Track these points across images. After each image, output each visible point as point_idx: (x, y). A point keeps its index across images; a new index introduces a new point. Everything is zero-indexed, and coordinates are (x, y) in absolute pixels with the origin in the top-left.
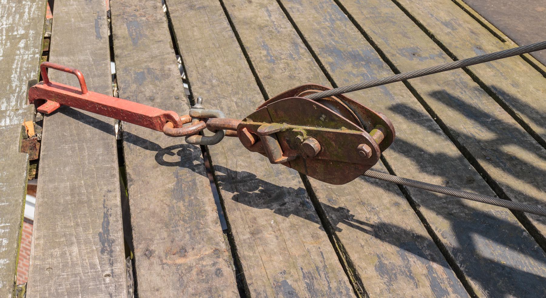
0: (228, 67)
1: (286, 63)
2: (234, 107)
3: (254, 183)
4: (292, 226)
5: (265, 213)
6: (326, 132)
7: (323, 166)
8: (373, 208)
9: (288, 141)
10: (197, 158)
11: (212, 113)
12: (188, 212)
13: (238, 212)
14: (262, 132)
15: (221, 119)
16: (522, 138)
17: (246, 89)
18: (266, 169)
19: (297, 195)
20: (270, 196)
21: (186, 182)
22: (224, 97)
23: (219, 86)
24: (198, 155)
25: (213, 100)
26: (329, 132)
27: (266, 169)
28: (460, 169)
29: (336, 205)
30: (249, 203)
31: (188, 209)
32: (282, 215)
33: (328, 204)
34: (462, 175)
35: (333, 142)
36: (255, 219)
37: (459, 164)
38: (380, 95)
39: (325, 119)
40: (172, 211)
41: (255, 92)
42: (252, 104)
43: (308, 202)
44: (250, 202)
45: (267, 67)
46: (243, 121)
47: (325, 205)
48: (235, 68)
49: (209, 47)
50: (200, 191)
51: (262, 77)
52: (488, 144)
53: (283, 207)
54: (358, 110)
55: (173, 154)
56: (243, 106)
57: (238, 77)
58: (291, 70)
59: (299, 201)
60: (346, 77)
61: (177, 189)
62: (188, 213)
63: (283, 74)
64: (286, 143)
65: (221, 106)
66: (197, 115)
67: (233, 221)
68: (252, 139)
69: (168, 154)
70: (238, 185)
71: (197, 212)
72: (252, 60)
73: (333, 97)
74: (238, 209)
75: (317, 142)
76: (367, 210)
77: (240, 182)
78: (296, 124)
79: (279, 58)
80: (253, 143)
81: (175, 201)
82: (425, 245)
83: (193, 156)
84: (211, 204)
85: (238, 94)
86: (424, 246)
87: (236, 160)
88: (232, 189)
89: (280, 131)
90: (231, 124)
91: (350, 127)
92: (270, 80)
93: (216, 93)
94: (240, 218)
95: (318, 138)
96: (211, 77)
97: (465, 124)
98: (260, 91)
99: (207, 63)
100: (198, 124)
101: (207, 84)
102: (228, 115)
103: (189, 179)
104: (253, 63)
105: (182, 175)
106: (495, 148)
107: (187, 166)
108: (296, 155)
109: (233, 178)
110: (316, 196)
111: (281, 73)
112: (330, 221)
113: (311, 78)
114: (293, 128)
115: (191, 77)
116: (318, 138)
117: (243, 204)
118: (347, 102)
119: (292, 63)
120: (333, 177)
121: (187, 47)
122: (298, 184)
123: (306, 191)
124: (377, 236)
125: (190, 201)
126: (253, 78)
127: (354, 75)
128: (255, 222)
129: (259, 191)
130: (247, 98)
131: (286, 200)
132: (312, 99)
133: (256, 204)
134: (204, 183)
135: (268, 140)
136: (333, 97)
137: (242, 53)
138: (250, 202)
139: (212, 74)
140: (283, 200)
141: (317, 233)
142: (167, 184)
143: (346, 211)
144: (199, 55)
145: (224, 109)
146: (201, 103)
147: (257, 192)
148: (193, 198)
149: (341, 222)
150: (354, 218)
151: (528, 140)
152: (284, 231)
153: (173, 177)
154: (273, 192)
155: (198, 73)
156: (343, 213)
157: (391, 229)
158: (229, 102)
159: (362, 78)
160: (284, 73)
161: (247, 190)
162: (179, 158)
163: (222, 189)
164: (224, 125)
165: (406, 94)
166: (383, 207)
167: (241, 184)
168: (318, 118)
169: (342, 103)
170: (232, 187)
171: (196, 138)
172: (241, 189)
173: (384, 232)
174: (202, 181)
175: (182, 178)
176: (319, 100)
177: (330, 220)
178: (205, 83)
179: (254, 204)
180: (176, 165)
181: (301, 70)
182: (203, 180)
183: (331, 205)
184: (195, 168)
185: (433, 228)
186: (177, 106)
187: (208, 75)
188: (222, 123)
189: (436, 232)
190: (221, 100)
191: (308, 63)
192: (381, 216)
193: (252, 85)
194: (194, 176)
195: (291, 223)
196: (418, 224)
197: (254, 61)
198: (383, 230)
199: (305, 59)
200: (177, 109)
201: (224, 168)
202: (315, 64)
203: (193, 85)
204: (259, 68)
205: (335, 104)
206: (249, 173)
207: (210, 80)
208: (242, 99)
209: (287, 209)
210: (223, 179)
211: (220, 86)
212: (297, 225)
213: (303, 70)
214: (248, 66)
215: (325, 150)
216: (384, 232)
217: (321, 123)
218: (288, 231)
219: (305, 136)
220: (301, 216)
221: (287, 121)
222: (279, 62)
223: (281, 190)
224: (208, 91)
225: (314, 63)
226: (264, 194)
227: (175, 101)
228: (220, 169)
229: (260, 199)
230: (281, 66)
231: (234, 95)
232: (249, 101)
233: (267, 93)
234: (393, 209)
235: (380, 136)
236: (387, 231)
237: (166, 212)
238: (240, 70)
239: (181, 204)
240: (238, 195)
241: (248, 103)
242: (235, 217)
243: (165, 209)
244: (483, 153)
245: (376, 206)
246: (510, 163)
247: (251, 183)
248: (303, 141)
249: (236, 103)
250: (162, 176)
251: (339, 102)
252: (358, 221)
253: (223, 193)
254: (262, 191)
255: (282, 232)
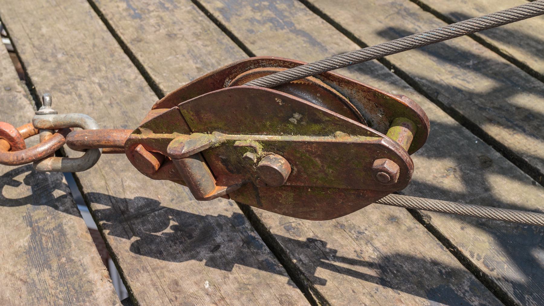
0: (75, 33)
1: (158, 16)
2: (98, 92)
3: (159, 216)
4: (242, 287)
5: (191, 270)
6: (304, 143)
7: (292, 194)
8: (360, 233)
9: (224, 161)
10: (58, 186)
11: (72, 121)
12: (61, 288)
13: (145, 275)
14: (177, 153)
15: (93, 131)
16: (527, 85)
17: (110, 63)
18: (171, 188)
19: (233, 226)
20: (190, 237)
21: (47, 231)
22: (80, 79)
23: (68, 62)
24: (57, 180)
25: (64, 85)
26: (309, 143)
27: (171, 188)
28: (463, 145)
29: (300, 236)
30: (159, 255)
31: (60, 284)
32: (220, 269)
33: (287, 235)
34: (470, 154)
35: (317, 159)
36: (176, 283)
37: (458, 136)
38: (305, 47)
39: (299, 121)
40: (33, 291)
41: (124, 65)
42: (124, 84)
43: (254, 238)
44: (161, 253)
45: (132, 26)
46: (134, 133)
47: (283, 238)
48: (86, 33)
49: (43, 7)
50: (73, 245)
51: (129, 41)
52: (485, 100)
53: (217, 254)
54: (357, 95)
55: (17, 184)
56: (111, 89)
57: (94, 45)
58: (167, 26)
59: (240, 238)
60: (249, 26)
61: (35, 248)
62: (61, 291)
63: (157, 33)
64: (220, 165)
65: (78, 93)
66: (47, 125)
67: (141, 293)
68: (155, 162)
69: (9, 184)
70: (134, 224)
71: (76, 286)
72: (108, 17)
73: (311, 78)
74: (144, 269)
75: (284, 161)
76: (351, 237)
77: (136, 217)
78: (238, 132)
79: (146, 11)
80: (157, 168)
81: (34, 271)
82: (467, 288)
83: (50, 183)
84: (98, 268)
85: (100, 70)
86: (466, 291)
87: (120, 179)
88: (126, 232)
89: (211, 148)
90: (111, 139)
91: (353, 131)
92: (141, 44)
93: (66, 72)
94: (151, 286)
95: (286, 154)
96: (54, 51)
97: (439, 74)
98: (130, 63)
99: (44, 30)
100: (51, 140)
101: (50, 62)
102: (92, 106)
103: (52, 226)
104: (111, 22)
105: (39, 219)
106: (496, 105)
107: (44, 201)
108: (240, 182)
109: (123, 212)
110: (263, 225)
111: (155, 32)
112: (301, 268)
113: (199, 34)
114: (235, 141)
115: (24, 53)
116: (286, 154)
117: (149, 258)
118: (335, 83)
119: (166, 15)
120: (313, 209)
121: (10, 10)
122: (229, 207)
123: (246, 219)
124: (383, 282)
125: (61, 267)
126: (116, 45)
127: (258, 22)
128: (178, 289)
129: (171, 228)
130: (114, 75)
131: (219, 239)
132: (268, 87)
133: (172, 254)
134: (78, 229)
135: (188, 164)
136: (311, 78)
137: (92, 11)
138: (161, 253)
139: (55, 45)
140: (214, 240)
141: (286, 295)
142: (16, 240)
143: (319, 245)
144: (31, 20)
145: (83, 97)
146: (50, 104)
147: (168, 230)
148: (64, 260)
149: (318, 266)
150: (338, 254)
151: (536, 86)
152: (230, 300)
153: (24, 225)
154: (193, 227)
155: (34, 46)
156: (315, 249)
157: (402, 267)
158: (88, 86)
159: (271, 24)
160: (159, 30)
161: (150, 230)
162: (28, 190)
163: (109, 234)
164: (98, 141)
165: (341, 40)
166: (374, 228)
167: (139, 220)
168: (285, 120)
169: (325, 86)
170: (124, 228)
171: (53, 163)
172: (140, 230)
173: (393, 273)
174: (73, 226)
175: (40, 225)
176: (280, 86)
177: (299, 265)
178: (46, 61)
179: (167, 255)
180: (26, 204)
181: (182, 23)
182: (76, 224)
183: (292, 238)
184: (57, 203)
185: (467, 254)
186: (10, 101)
187: (49, 48)
188: (96, 138)
189: (474, 261)
190: (76, 82)
191: (189, 12)
192: (378, 244)
193: (116, 54)
194: (59, 218)
195: (238, 282)
196: (439, 250)
197: (111, 19)
198: (390, 269)
199: (183, 7)
200: (11, 106)
201: (105, 195)
202: (199, 13)
203: (29, 65)
204: (120, 28)
205: (313, 89)
206: (147, 199)
207: (54, 56)
208: (107, 78)
209: (224, 256)
210: (106, 216)
211: (71, 62)
212: (250, 285)
213: (185, 23)
214: (105, 28)
215: (299, 171)
216: (393, 273)
217: (291, 127)
218: (239, 299)
219: (260, 152)
220: (251, 266)
221: (221, 128)
222: (147, 16)
223: (205, 221)
224: (54, 72)
225: (197, 11)
226: (179, 233)
227: (7, 94)
228: (98, 197)
229: (176, 243)
230: (152, 21)
231: (94, 73)
232: (119, 80)
233: (143, 63)
234: (391, 228)
235: (408, 137)
236: (397, 271)
237: (22, 296)
238: (94, 35)
239: (46, 275)
240: (137, 241)
241: (117, 83)
242: (143, 284)
243: (19, 289)
244: (484, 114)
245: (363, 228)
246: (529, 125)
247: (153, 217)
248: (258, 162)
249: (100, 85)
250: (5, 226)
251: (320, 86)
252: (344, 260)
253: (112, 240)
254: (174, 228)
255: (228, 301)
